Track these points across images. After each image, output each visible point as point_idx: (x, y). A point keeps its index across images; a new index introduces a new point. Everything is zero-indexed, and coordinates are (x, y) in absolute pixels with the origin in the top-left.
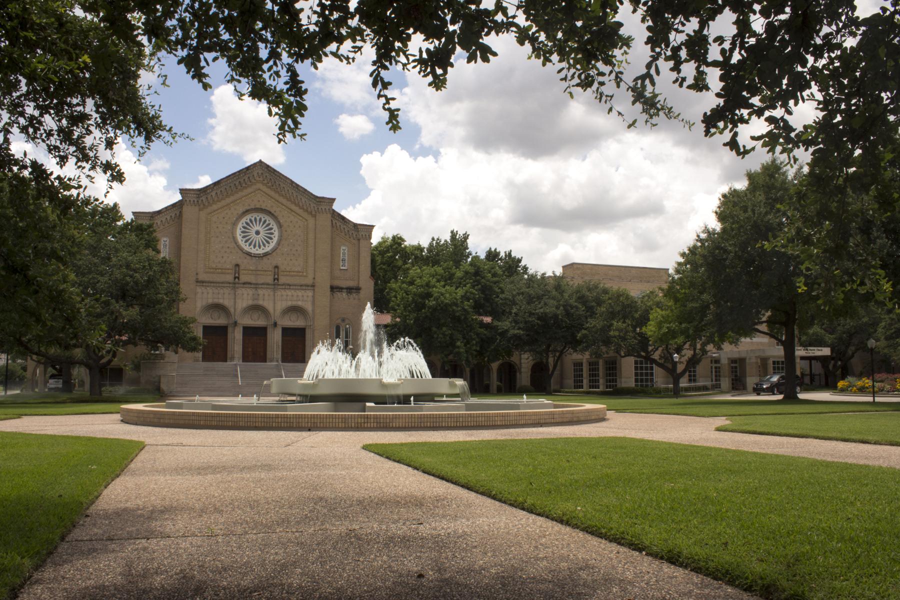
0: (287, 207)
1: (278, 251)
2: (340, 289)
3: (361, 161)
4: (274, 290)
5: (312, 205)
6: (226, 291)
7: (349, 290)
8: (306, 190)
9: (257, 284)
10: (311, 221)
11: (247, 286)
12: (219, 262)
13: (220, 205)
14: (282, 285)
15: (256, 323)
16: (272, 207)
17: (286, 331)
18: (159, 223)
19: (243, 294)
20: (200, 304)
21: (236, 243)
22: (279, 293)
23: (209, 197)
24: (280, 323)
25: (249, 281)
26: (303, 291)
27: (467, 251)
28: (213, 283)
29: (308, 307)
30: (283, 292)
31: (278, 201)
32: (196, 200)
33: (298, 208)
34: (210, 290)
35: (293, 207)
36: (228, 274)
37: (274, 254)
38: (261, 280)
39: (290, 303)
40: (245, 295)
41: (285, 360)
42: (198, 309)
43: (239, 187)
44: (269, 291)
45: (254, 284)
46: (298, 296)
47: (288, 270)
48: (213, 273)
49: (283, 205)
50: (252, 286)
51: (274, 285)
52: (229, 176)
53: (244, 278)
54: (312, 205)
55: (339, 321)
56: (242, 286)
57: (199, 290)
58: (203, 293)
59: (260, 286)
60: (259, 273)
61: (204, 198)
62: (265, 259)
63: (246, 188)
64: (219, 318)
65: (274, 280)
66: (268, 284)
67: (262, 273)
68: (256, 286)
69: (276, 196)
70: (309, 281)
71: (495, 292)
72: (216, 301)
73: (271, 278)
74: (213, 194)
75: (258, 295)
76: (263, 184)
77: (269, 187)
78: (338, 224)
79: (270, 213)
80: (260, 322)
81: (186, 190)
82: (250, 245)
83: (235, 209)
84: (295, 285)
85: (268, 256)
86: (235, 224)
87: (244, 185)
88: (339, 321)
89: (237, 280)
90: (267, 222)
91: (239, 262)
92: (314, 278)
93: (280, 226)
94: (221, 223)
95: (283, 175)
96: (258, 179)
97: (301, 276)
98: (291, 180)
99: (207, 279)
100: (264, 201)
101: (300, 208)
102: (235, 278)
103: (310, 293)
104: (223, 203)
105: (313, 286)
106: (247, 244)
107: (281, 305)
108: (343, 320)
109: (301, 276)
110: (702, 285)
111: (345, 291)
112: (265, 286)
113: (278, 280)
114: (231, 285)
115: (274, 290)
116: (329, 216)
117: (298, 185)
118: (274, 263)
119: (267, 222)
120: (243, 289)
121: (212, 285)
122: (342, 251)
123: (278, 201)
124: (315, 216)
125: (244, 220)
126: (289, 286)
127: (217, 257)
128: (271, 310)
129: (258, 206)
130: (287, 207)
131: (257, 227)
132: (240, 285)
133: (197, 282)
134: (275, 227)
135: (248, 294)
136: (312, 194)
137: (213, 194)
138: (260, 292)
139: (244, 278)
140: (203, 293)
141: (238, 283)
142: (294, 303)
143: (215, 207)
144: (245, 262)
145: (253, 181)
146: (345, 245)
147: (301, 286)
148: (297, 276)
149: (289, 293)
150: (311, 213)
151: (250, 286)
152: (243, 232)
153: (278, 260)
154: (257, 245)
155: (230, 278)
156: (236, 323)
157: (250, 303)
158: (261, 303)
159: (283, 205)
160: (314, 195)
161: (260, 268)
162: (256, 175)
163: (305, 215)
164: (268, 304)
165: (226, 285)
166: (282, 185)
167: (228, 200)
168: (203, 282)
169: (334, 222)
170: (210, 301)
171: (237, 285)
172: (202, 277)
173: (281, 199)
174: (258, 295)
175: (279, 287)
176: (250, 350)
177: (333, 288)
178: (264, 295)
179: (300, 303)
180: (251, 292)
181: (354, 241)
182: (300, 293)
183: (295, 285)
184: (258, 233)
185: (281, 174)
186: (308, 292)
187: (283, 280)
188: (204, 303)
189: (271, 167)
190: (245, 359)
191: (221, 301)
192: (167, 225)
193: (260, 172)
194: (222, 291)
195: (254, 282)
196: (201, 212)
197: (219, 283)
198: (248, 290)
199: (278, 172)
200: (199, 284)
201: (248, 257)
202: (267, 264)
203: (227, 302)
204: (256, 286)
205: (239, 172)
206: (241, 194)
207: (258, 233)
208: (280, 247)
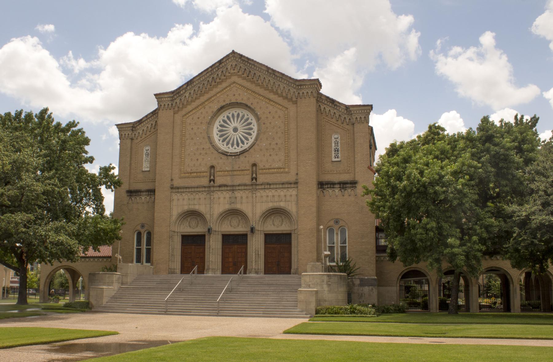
0: (265, 97)
1: (256, 147)
2: (332, 184)
3: (546, 131)
4: (209, 192)
5: (292, 90)
6: (202, 196)
7: (343, 185)
8: (283, 75)
9: (233, 186)
10: (292, 109)
11: (223, 188)
12: (194, 165)
13: (194, 105)
14: (262, 185)
15: (194, 230)
16: (249, 99)
17: (227, 238)
18: (141, 132)
19: (219, 198)
20: (176, 212)
21: (211, 143)
22: (258, 194)
23: (183, 98)
24: (258, 227)
25: (225, 183)
26: (285, 190)
27: (538, 138)
28: (189, 188)
29: (292, 208)
30: (263, 193)
31: (254, 92)
32: (170, 104)
33: (276, 96)
34: (186, 196)
35: (272, 96)
36: (203, 177)
37: (251, 150)
38: (237, 181)
39: (271, 205)
40: (222, 199)
41: (267, 271)
42: (174, 218)
43: (213, 83)
44: (247, 192)
45: (230, 186)
46: (279, 196)
47: (267, 167)
48: (188, 177)
49: (260, 95)
50: (229, 188)
51: (252, 185)
52: (202, 73)
53: (219, 181)
54: (292, 90)
55: (332, 223)
56: (218, 189)
57: (175, 197)
58: (178, 200)
59: (237, 188)
60: (235, 173)
61: (178, 101)
62: (242, 157)
63: (220, 83)
64: (197, 226)
65: (252, 180)
66: (245, 185)
67: (238, 173)
68: (232, 188)
69: (253, 87)
70: (291, 178)
71: (514, 162)
72: (192, 207)
73: (249, 177)
74: (187, 95)
75: (236, 198)
76: (239, 76)
77: (244, 79)
78: (327, 109)
79: (247, 106)
80: (239, 229)
81: (160, 94)
82: (227, 144)
83: (210, 107)
84: (276, 184)
85: (245, 154)
86: (210, 123)
87: (218, 80)
88: (332, 223)
89: (212, 183)
90: (246, 117)
91: (214, 163)
92: (297, 174)
93: (258, 119)
94: (195, 124)
95: (258, 63)
96: (232, 71)
97: (282, 173)
98: (267, 67)
99: (182, 185)
100: (239, 95)
101: (279, 96)
102: (210, 181)
103: (293, 192)
104: (198, 102)
105: (296, 183)
106: (230, 145)
107: (261, 208)
108: (337, 222)
109: (282, 173)
110: (478, 244)
111: (338, 186)
112: (243, 188)
113: (256, 179)
114: (206, 189)
115: (209, 192)
116: (313, 100)
117: (274, 71)
118: (252, 161)
119: (246, 117)
120: (219, 193)
121: (188, 190)
122: (333, 140)
123: (254, 92)
124: (295, 103)
125: (221, 118)
126: (269, 185)
127: (192, 160)
128: (250, 215)
129: (233, 101)
130: (265, 97)
131: (234, 124)
132: (215, 189)
133: (172, 188)
134: (254, 122)
135: (225, 198)
136: (290, 78)
137: (187, 95)
138: (238, 194)
139: (219, 181)
140: (178, 200)
141: (214, 187)
142: (276, 205)
143: (189, 108)
144: (222, 164)
145: (227, 74)
146: (336, 133)
147: (283, 184)
148: (278, 173)
149: (270, 193)
150: (291, 100)
151: (226, 188)
152: (220, 131)
153: (256, 157)
154: (243, 139)
155: (205, 181)
156: (252, 230)
157: (227, 207)
158: (238, 206)
159: (260, 95)
160: (293, 79)
161: (236, 168)
162: (229, 67)
163: (285, 103)
164: (245, 208)
165: (201, 190)
166: (258, 74)
167: (202, 99)
168: (178, 188)
169: (322, 107)
170: (186, 208)
171: (212, 189)
172: (176, 183)
173: (258, 89)
174: (236, 198)
175: (258, 187)
176: (230, 260)
177: (321, 185)
178: (242, 197)
179: (282, 204)
180: (227, 195)
181: (347, 127)
182: (282, 193)
183: (276, 184)
184: (235, 130)
185: (255, 62)
186: (291, 190)
187: (261, 179)
188: (180, 210)
189: (244, 57)
190: (225, 270)
191: (197, 207)
192: (148, 133)
193: (234, 64)
194: (197, 196)
195: (230, 184)
196: (176, 115)
197: (194, 188)
198: (224, 193)
199: (253, 60)
200: (174, 191)
201: (224, 157)
202: (244, 163)
203: (202, 209)
204: (232, 188)
205: (211, 67)
206: (215, 90)
207: (235, 130)
208: (258, 142)
